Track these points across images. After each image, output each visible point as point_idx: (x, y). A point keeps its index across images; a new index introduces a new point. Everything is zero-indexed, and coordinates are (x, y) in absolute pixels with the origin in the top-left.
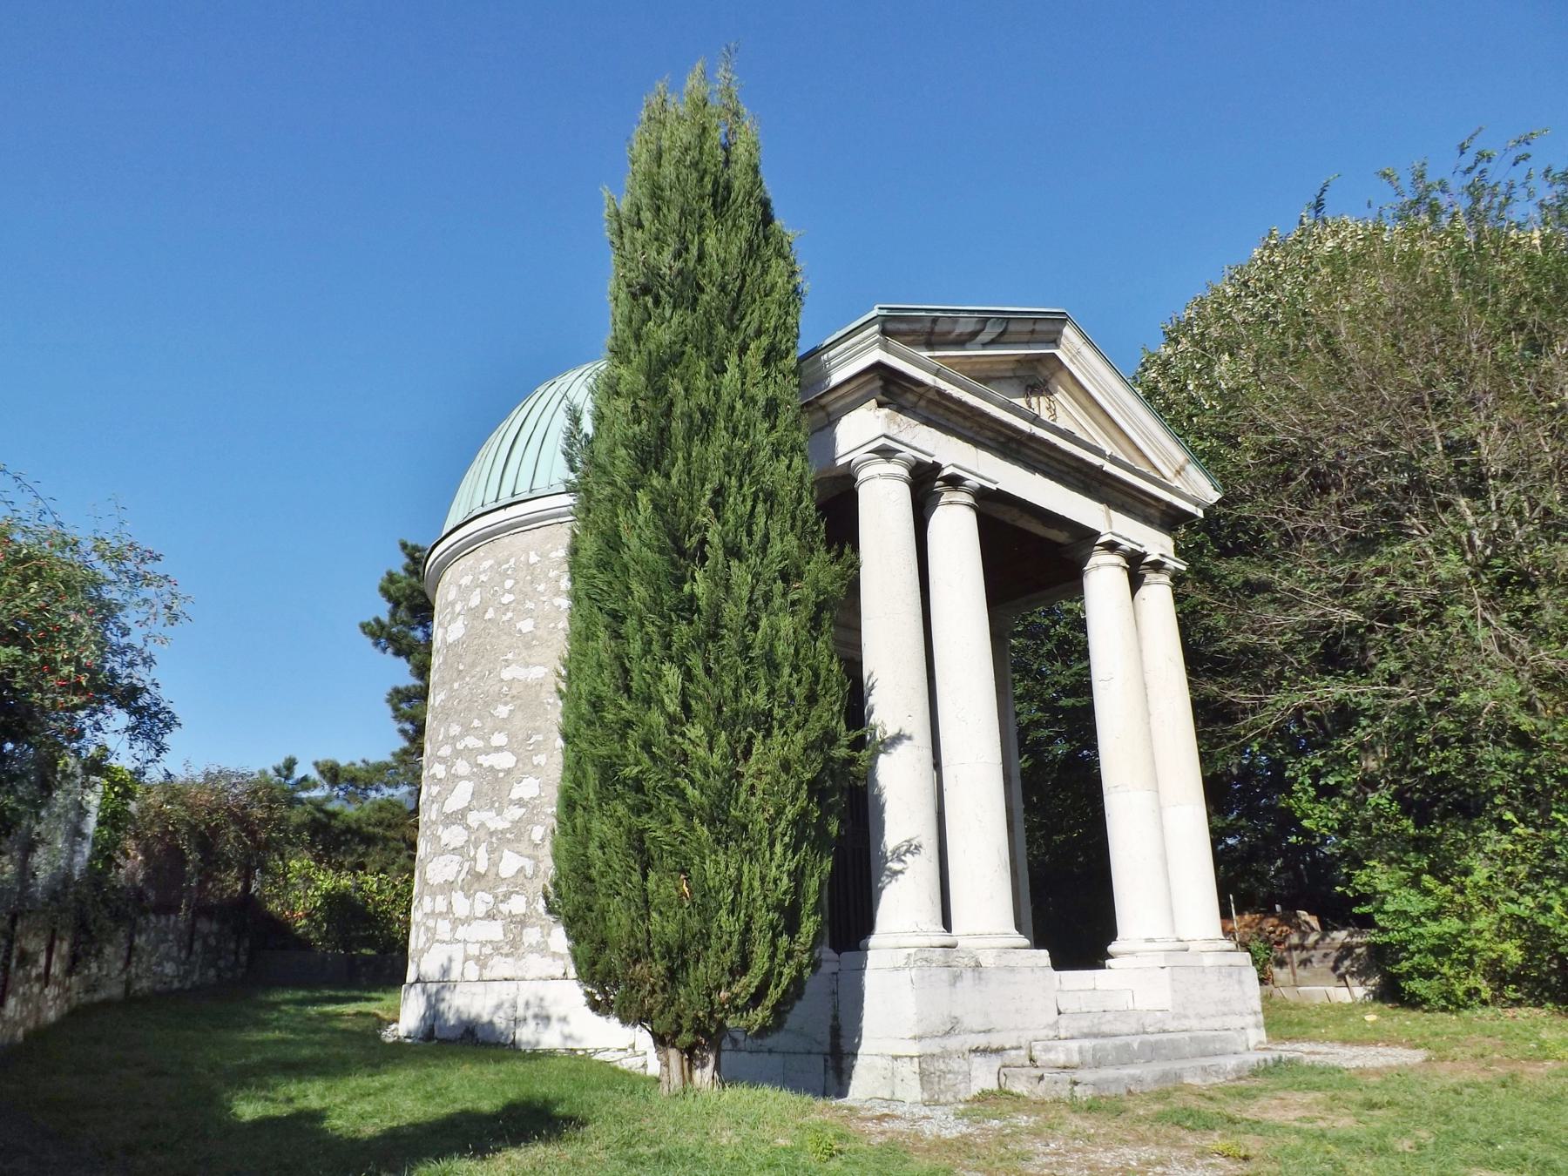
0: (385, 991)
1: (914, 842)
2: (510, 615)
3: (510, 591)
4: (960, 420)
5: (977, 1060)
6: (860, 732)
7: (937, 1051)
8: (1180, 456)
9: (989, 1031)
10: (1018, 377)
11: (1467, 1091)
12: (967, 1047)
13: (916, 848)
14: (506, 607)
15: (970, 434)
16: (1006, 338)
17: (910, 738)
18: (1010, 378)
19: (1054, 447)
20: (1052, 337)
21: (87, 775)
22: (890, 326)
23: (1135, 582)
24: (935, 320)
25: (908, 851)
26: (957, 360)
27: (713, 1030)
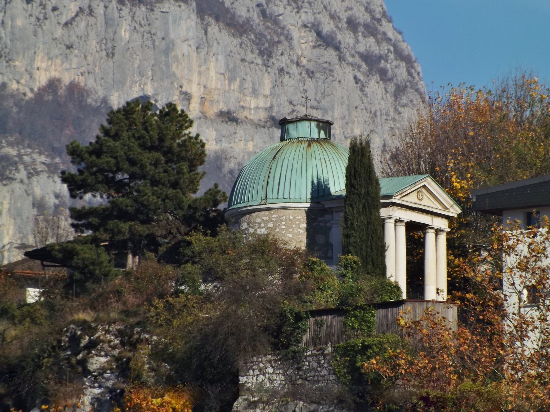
0: (197, 13)
2: (284, 232)
3: (284, 225)
5: (209, 34)
8: (452, 203)
11: (238, 353)
14: (283, 229)
21: (365, 354)
23: (437, 235)
27: (348, 359)
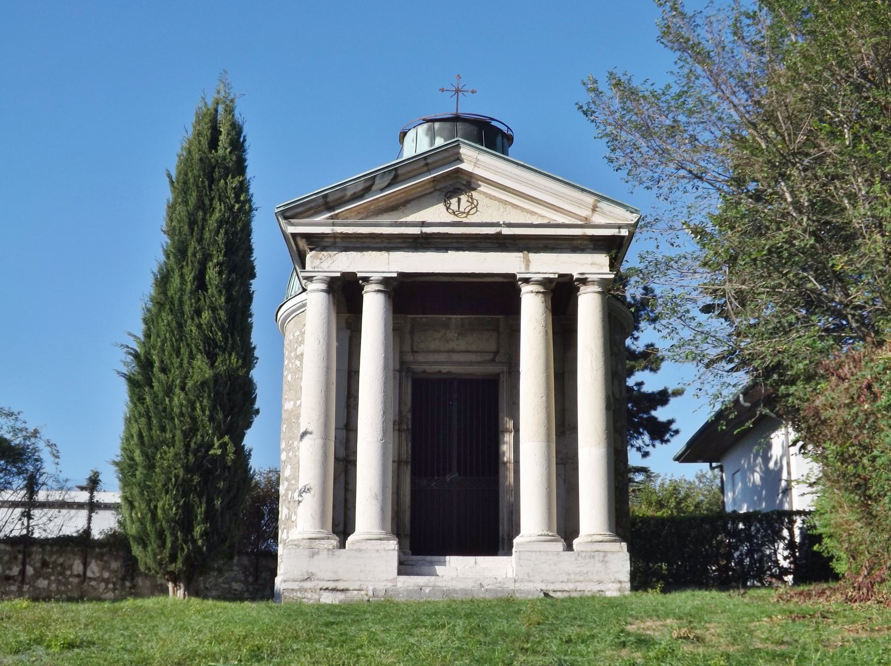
1: (307, 487)
4: (371, 240)
6: (221, 441)
7: (297, 587)
9: (337, 580)
10: (439, 190)
12: (319, 587)
13: (308, 490)
15: (383, 245)
16: (400, 178)
17: (311, 433)
18: (431, 193)
19: (446, 235)
20: (456, 157)
22: (288, 214)
24: (325, 196)
25: (304, 491)
26: (368, 204)
